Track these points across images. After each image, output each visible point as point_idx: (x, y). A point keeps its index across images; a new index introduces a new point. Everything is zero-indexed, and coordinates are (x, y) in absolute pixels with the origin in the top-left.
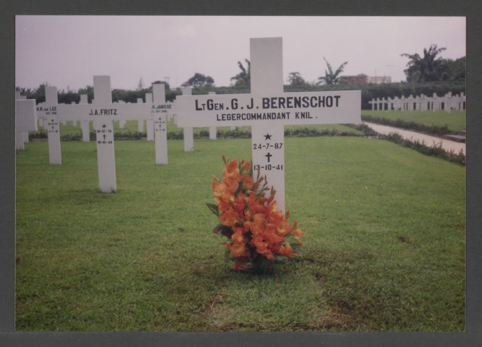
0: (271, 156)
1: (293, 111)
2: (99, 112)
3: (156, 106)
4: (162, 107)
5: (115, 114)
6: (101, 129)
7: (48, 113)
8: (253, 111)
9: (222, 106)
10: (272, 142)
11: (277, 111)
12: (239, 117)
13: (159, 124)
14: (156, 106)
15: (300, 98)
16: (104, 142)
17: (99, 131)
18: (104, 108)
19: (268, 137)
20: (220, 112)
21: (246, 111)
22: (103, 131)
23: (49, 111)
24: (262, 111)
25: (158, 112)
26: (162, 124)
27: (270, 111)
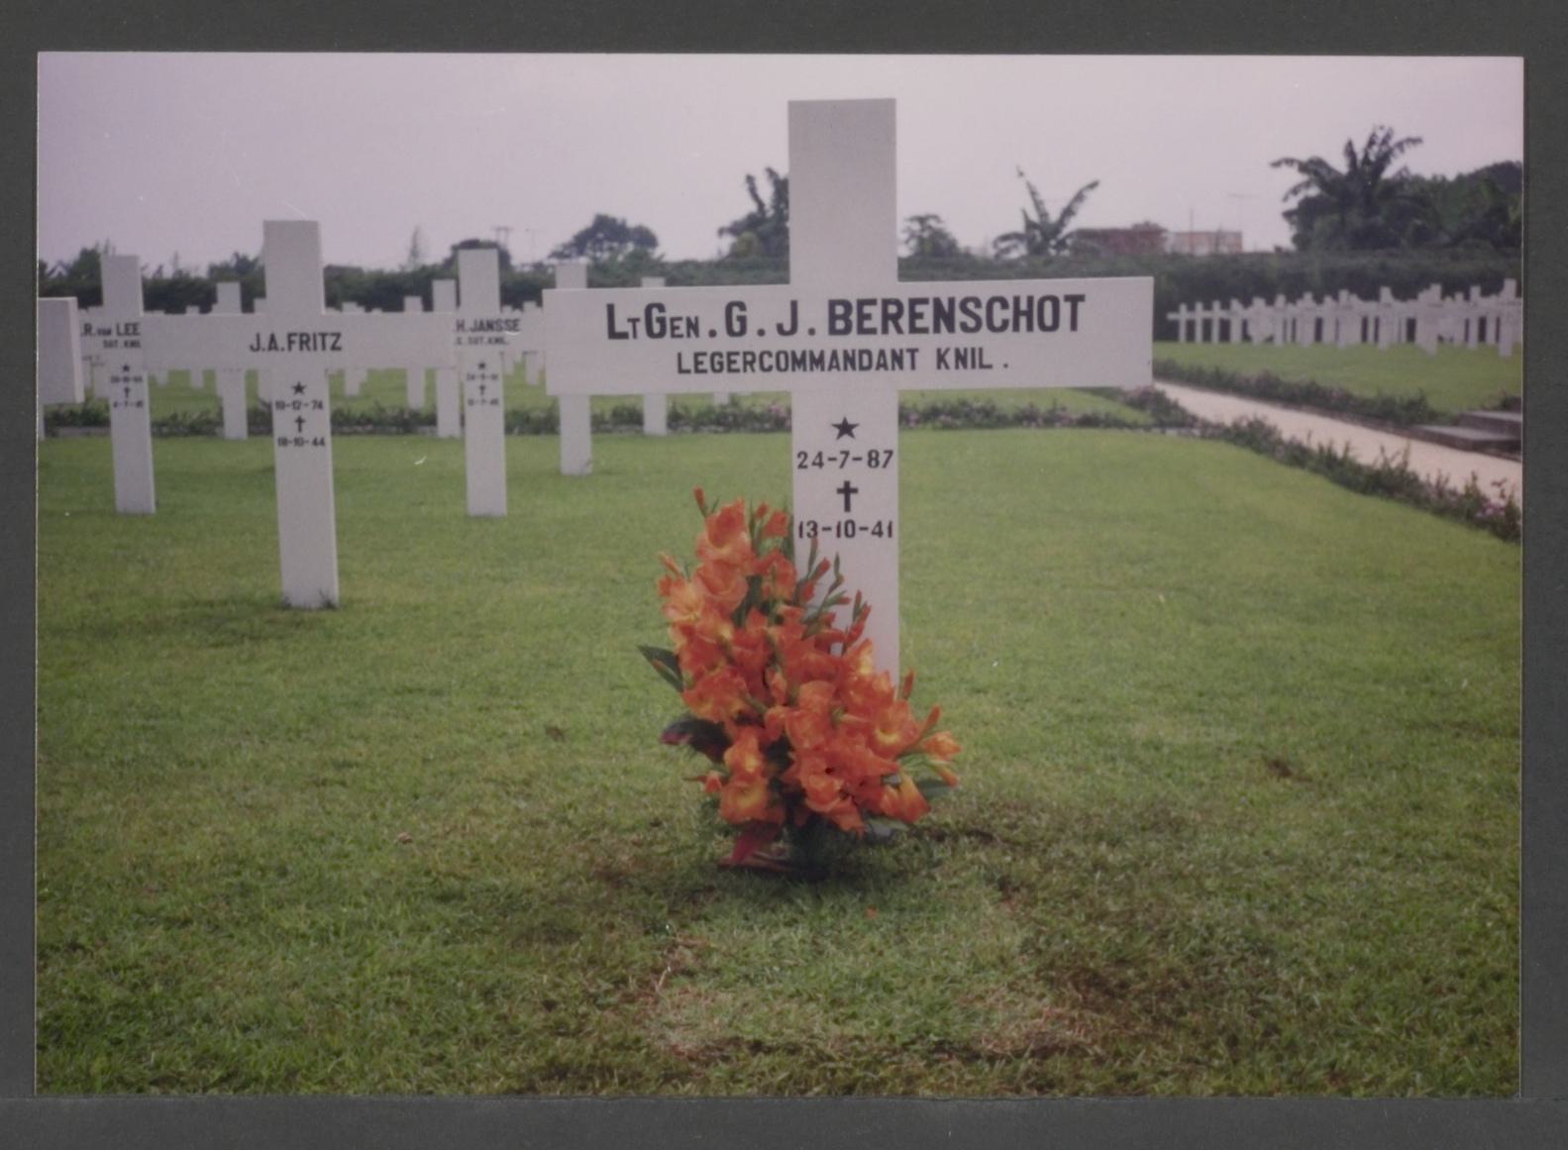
0: (855, 491)
1: (928, 344)
2: (282, 342)
3: (469, 324)
4: (490, 326)
5: (334, 348)
6: (289, 396)
7: (109, 345)
8: (798, 344)
9: (693, 326)
10: (857, 445)
11: (875, 343)
12: (751, 361)
13: (478, 382)
14: (469, 324)
15: (951, 301)
16: (298, 442)
17: (281, 405)
18: (299, 330)
19: (845, 429)
20: (688, 346)
21: (775, 343)
22: (296, 405)
23: (113, 336)
24: (825, 344)
25: (474, 341)
26: (488, 383)
27: (853, 342)
